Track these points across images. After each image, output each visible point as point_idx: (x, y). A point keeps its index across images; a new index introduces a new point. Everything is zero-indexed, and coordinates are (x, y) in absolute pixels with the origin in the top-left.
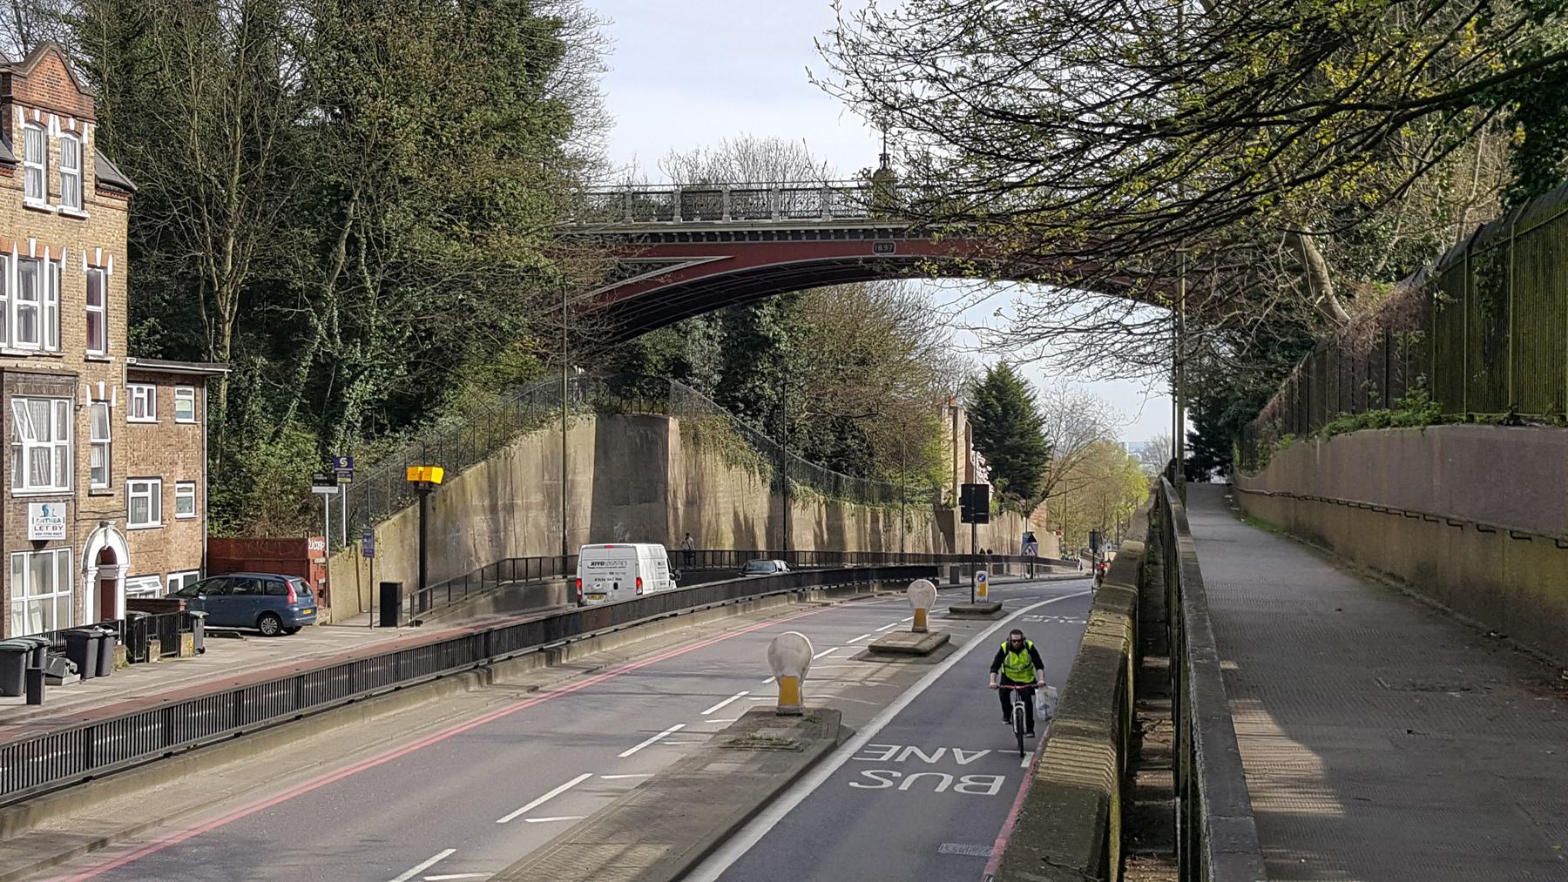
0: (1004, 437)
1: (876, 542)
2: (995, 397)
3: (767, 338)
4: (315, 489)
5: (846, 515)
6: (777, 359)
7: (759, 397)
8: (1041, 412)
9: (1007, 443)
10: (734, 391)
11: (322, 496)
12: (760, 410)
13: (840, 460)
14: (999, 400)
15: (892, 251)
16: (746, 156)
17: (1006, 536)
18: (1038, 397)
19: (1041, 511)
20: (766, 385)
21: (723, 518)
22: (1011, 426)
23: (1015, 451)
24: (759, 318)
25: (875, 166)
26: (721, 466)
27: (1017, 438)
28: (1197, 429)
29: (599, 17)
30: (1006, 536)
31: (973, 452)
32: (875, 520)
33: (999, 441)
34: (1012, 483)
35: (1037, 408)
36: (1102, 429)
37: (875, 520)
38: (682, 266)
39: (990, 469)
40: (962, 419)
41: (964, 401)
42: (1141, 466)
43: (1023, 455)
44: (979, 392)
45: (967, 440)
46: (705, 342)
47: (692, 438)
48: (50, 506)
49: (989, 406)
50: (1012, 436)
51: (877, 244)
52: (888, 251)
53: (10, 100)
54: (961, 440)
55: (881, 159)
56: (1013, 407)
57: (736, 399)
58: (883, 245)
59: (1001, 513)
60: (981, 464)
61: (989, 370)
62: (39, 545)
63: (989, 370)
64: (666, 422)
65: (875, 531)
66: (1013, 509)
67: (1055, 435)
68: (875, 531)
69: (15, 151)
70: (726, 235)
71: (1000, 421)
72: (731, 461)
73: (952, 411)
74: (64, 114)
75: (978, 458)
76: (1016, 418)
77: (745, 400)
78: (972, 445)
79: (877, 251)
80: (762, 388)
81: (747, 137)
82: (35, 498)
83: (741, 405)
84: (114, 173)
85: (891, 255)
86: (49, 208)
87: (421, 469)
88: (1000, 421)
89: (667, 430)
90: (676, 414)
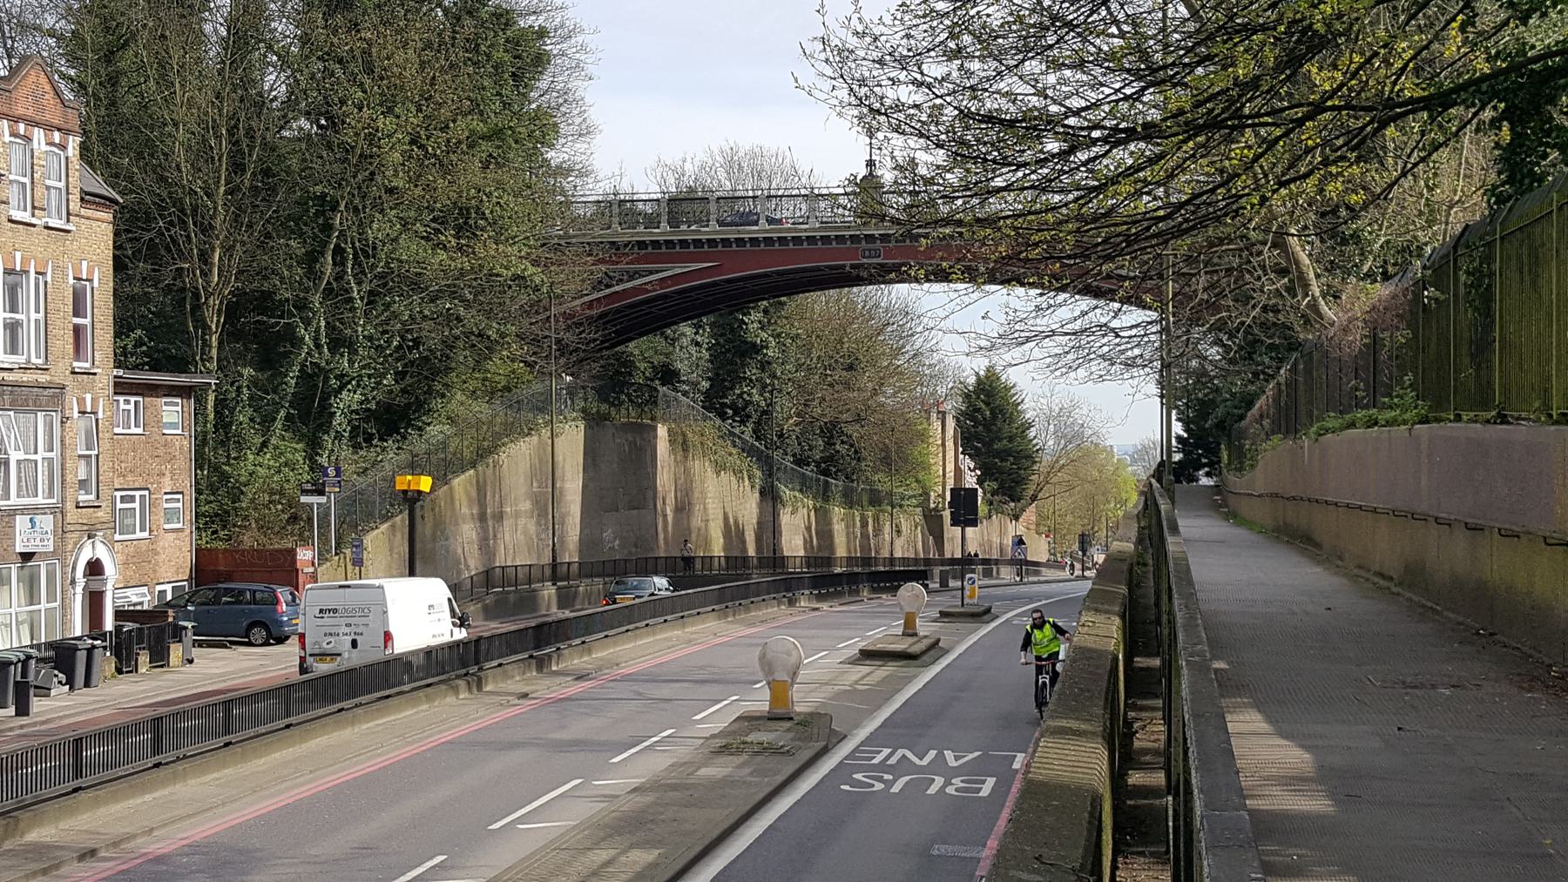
0: (992, 441)
1: (865, 547)
3: (754, 345)
4: (304, 499)
5: (835, 521)
6: (765, 365)
7: (748, 403)
8: (1029, 415)
9: (996, 447)
10: (721, 398)
11: (310, 506)
12: (749, 416)
13: (829, 465)
14: (987, 404)
15: (879, 256)
17: (996, 540)
19: (1030, 514)
21: (712, 524)
23: (1004, 455)
24: (746, 324)
25: (862, 172)
27: (1005, 442)
28: (1185, 431)
30: (996, 540)
31: (961, 456)
32: (864, 524)
33: (988, 444)
34: (1001, 487)
37: (864, 524)
39: (979, 472)
40: (951, 423)
42: (1130, 468)
43: (1011, 459)
45: (956, 444)
46: (693, 349)
47: (681, 444)
48: (38, 518)
49: (978, 410)
50: (1000, 440)
51: (864, 250)
52: (875, 257)
54: (950, 444)
55: (867, 165)
56: (1001, 411)
57: (724, 405)
59: (990, 517)
60: (969, 468)
61: (977, 374)
62: (27, 557)
63: (977, 374)
64: (655, 429)
65: (865, 536)
66: (1002, 513)
67: (1044, 438)
68: (865, 536)
70: (712, 242)
71: (987, 425)
72: (719, 468)
73: (940, 416)
76: (1005, 421)
77: (733, 406)
82: (23, 510)
83: (730, 412)
85: (879, 260)
88: (987, 425)
89: (656, 437)
90: (664, 421)
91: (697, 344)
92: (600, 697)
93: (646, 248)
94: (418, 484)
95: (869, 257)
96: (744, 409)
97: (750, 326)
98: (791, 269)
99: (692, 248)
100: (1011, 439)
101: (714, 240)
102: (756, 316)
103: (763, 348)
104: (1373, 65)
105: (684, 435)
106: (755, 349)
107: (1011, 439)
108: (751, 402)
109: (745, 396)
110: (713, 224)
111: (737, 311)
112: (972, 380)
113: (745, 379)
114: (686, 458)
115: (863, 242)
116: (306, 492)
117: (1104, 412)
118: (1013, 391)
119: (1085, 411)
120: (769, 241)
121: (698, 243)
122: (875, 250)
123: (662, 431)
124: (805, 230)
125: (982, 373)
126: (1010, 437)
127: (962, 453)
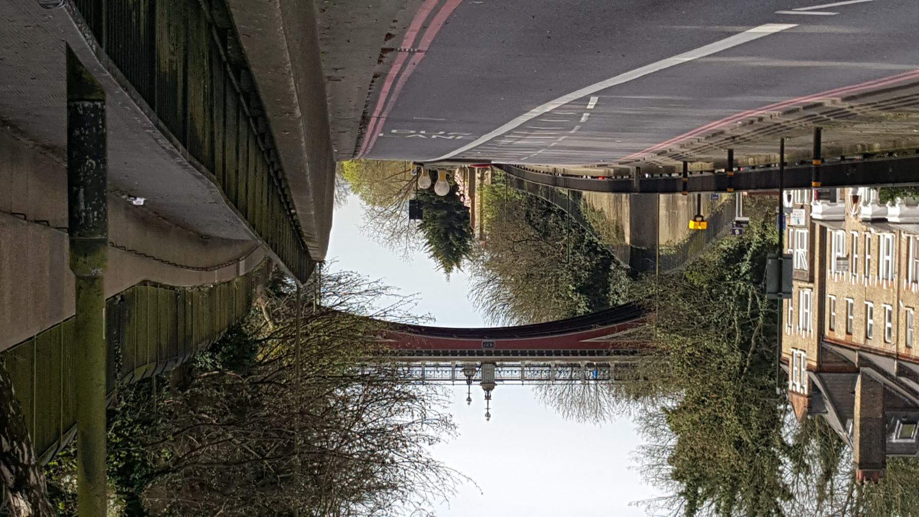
0: (448, 215)
2: (454, 246)
3: (581, 293)
4: (747, 219)
6: (577, 278)
7: (587, 254)
8: (421, 234)
9: (446, 212)
10: (605, 258)
11: (744, 215)
14: (451, 244)
16: (597, 411)
18: (423, 244)
20: (583, 262)
22: (442, 224)
24: (587, 306)
25: (492, 393)
26: (606, 210)
27: (439, 215)
29: (639, 475)
31: (469, 206)
33: (450, 214)
35: (426, 237)
36: (378, 220)
38: (609, 336)
39: (457, 194)
41: (473, 244)
43: (434, 202)
44: (467, 250)
46: (620, 291)
47: (619, 230)
48: (796, 224)
49: (458, 239)
50: (442, 217)
53: (808, 397)
54: (477, 216)
58: (489, 347)
61: (459, 267)
62: (802, 207)
63: (459, 267)
69: (807, 375)
70: (583, 354)
71: (450, 229)
74: (796, 393)
75: (467, 203)
76: (438, 231)
78: (470, 211)
79: (493, 343)
80: (586, 260)
81: (597, 424)
82: (801, 227)
84: (784, 367)
85: (484, 340)
86: (801, 352)
87: (700, 228)
88: (450, 229)
89: (630, 237)
90: (626, 246)
91: (617, 293)
92: (246, 157)
93: (581, 351)
94: (695, 225)
95: (489, 343)
96: (590, 250)
97: (584, 304)
98: (443, 336)
99: (553, 351)
100: (434, 218)
101: (582, 355)
102: (580, 311)
103: (576, 291)
104: (321, 512)
105: (617, 236)
106: (580, 290)
107: (434, 218)
108: (585, 255)
109: (588, 259)
110: (612, 365)
111: (593, 314)
112: (465, 261)
113: (589, 270)
114: (617, 222)
115: (493, 352)
116: (747, 222)
117: (366, 233)
118: (432, 253)
119: (382, 236)
120: (549, 354)
121: (591, 354)
122: (486, 347)
123: (628, 240)
124: (527, 359)
125: (455, 268)
126: (435, 219)
127: (469, 208)
